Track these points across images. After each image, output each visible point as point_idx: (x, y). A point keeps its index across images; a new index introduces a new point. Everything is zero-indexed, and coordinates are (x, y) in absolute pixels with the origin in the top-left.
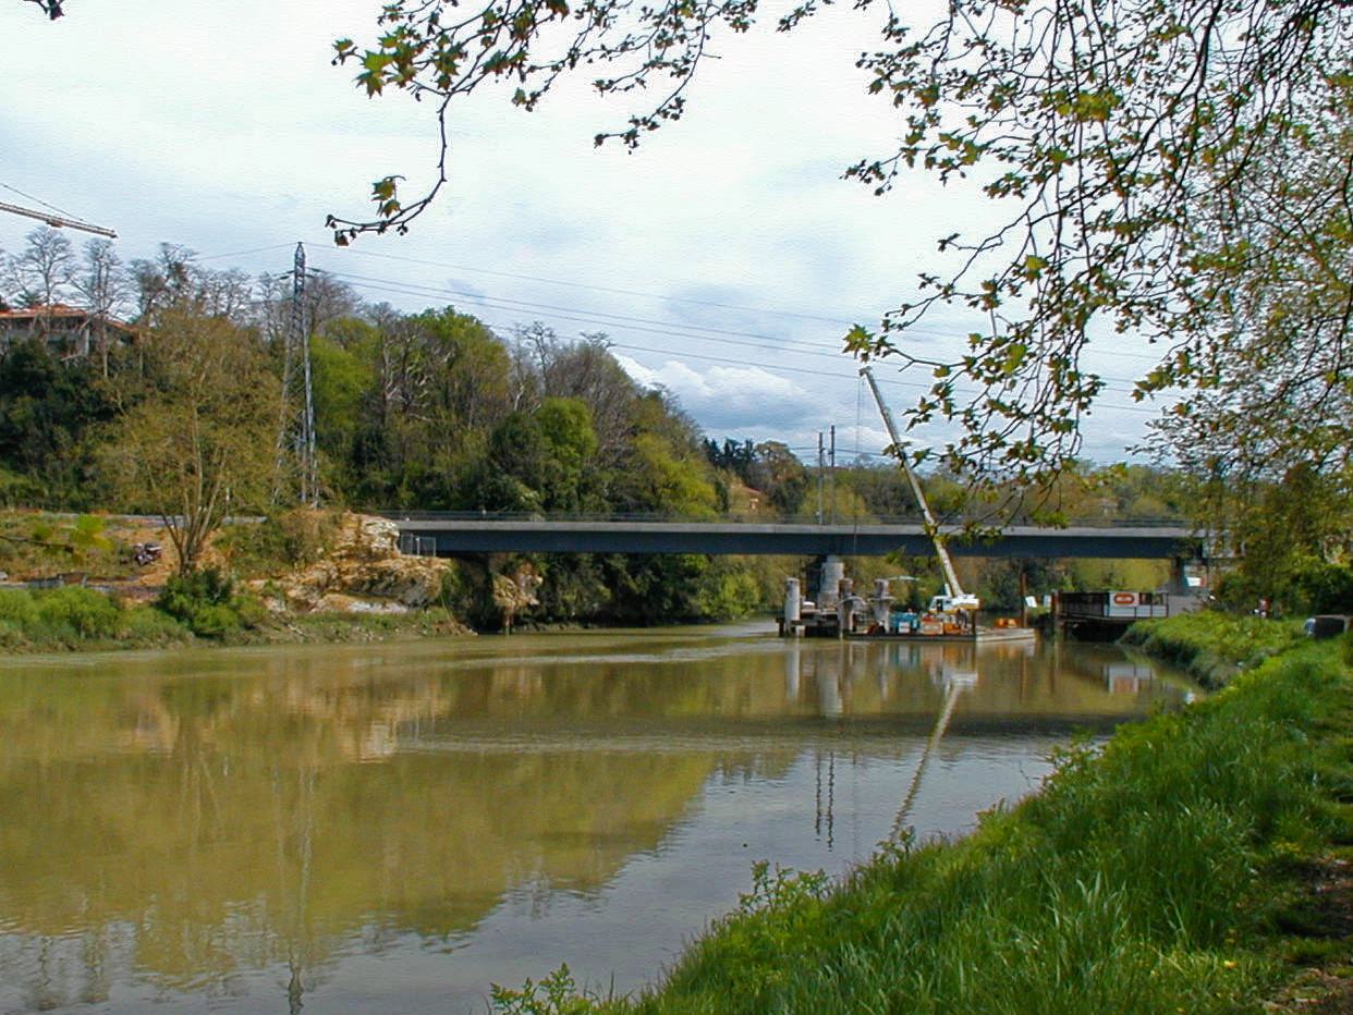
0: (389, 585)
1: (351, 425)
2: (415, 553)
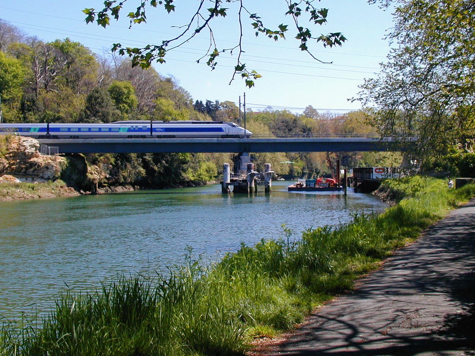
0: (35, 170)
1: (20, 95)
2: (48, 154)
